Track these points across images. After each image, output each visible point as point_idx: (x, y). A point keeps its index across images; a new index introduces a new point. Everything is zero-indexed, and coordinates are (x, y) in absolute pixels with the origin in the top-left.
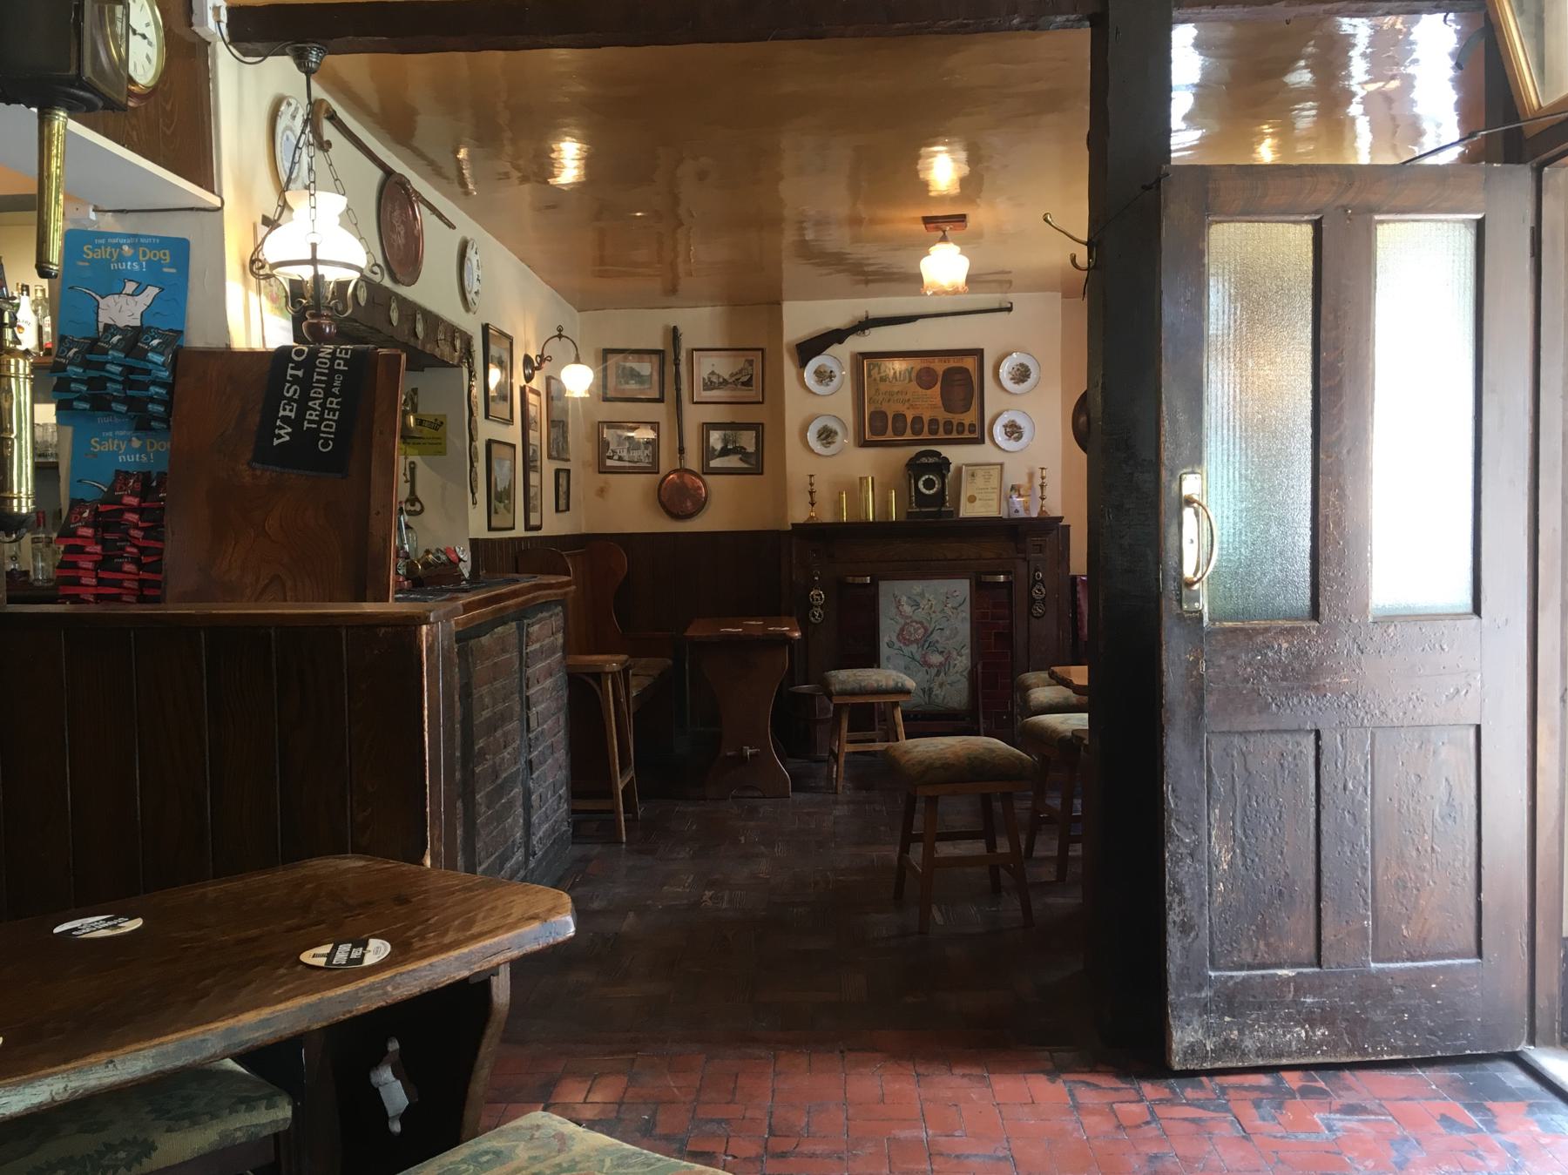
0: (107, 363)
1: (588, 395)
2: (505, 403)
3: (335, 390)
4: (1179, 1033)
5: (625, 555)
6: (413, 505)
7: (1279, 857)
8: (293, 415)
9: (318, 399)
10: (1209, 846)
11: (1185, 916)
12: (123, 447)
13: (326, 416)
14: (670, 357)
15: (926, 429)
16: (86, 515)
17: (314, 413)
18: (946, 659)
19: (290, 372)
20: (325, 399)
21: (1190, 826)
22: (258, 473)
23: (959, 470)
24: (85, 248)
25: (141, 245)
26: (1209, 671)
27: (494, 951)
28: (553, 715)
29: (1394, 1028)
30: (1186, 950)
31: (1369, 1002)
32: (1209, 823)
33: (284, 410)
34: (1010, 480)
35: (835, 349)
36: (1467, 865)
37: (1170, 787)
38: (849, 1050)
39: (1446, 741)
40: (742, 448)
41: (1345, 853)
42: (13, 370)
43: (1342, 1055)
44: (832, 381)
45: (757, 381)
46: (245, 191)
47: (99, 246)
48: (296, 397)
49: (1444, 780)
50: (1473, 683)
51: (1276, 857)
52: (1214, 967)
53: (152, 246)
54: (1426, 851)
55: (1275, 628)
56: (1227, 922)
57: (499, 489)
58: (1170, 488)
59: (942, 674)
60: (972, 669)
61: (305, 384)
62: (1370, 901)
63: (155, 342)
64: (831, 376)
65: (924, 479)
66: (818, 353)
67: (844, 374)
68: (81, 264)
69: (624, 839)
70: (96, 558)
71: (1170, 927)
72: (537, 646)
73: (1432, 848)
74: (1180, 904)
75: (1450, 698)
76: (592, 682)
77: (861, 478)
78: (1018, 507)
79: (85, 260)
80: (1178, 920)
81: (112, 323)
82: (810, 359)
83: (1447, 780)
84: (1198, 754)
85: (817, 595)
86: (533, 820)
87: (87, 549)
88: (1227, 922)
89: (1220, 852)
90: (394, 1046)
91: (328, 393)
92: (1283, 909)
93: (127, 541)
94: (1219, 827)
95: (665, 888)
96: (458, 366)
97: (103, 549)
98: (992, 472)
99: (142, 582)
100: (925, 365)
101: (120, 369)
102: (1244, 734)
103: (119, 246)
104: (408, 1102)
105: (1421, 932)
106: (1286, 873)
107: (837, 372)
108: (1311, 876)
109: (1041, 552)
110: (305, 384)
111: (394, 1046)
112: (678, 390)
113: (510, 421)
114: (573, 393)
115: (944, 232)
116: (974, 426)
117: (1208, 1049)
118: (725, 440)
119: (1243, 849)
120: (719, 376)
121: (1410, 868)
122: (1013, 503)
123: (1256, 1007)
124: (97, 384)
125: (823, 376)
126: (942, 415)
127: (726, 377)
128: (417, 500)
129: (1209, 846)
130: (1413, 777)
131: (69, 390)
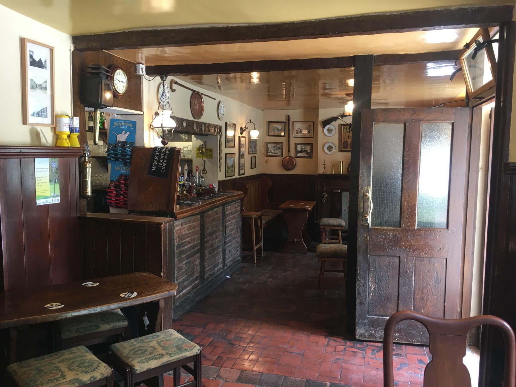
0: (118, 150)
1: (257, 139)
2: (232, 142)
3: (166, 158)
5: (271, 180)
6: (204, 171)
7: (388, 288)
8: (156, 163)
9: (162, 160)
12: (121, 169)
13: (163, 164)
14: (287, 123)
16: (113, 184)
19: (156, 153)
21: (363, 278)
24: (114, 123)
25: (126, 122)
27: (157, 297)
28: (235, 229)
29: (418, 336)
31: (411, 328)
32: (369, 278)
33: (155, 162)
35: (334, 123)
36: (442, 295)
37: (358, 268)
38: (281, 325)
39: (437, 262)
41: (406, 289)
42: (87, 166)
43: (403, 341)
44: (332, 132)
46: (150, 108)
47: (117, 123)
49: (436, 273)
50: (445, 247)
51: (387, 288)
52: (368, 315)
53: (128, 123)
54: (430, 290)
55: (389, 229)
56: (373, 304)
57: (229, 166)
61: (159, 156)
62: (413, 302)
63: (128, 145)
64: (332, 131)
66: (329, 124)
67: (336, 131)
68: (113, 126)
69: (256, 262)
70: (115, 194)
71: (357, 303)
72: (230, 212)
73: (432, 290)
75: (438, 251)
76: (249, 220)
79: (114, 126)
80: (359, 302)
82: (326, 126)
83: (437, 272)
84: (366, 260)
85: (325, 194)
86: (226, 257)
87: (113, 192)
88: (373, 304)
89: (371, 286)
90: (146, 313)
91: (164, 159)
92: (388, 302)
93: (121, 191)
95: (260, 277)
96: (217, 135)
97: (116, 192)
99: (124, 200)
101: (121, 152)
102: (379, 256)
103: (122, 123)
104: (149, 323)
105: (427, 312)
106: (389, 292)
108: (396, 294)
110: (159, 156)
111: (146, 313)
112: (289, 133)
113: (234, 147)
114: (253, 138)
117: (366, 335)
119: (378, 285)
121: (425, 295)
123: (379, 326)
124: (116, 155)
125: (329, 131)
128: (205, 170)
130: (427, 271)
131: (110, 156)
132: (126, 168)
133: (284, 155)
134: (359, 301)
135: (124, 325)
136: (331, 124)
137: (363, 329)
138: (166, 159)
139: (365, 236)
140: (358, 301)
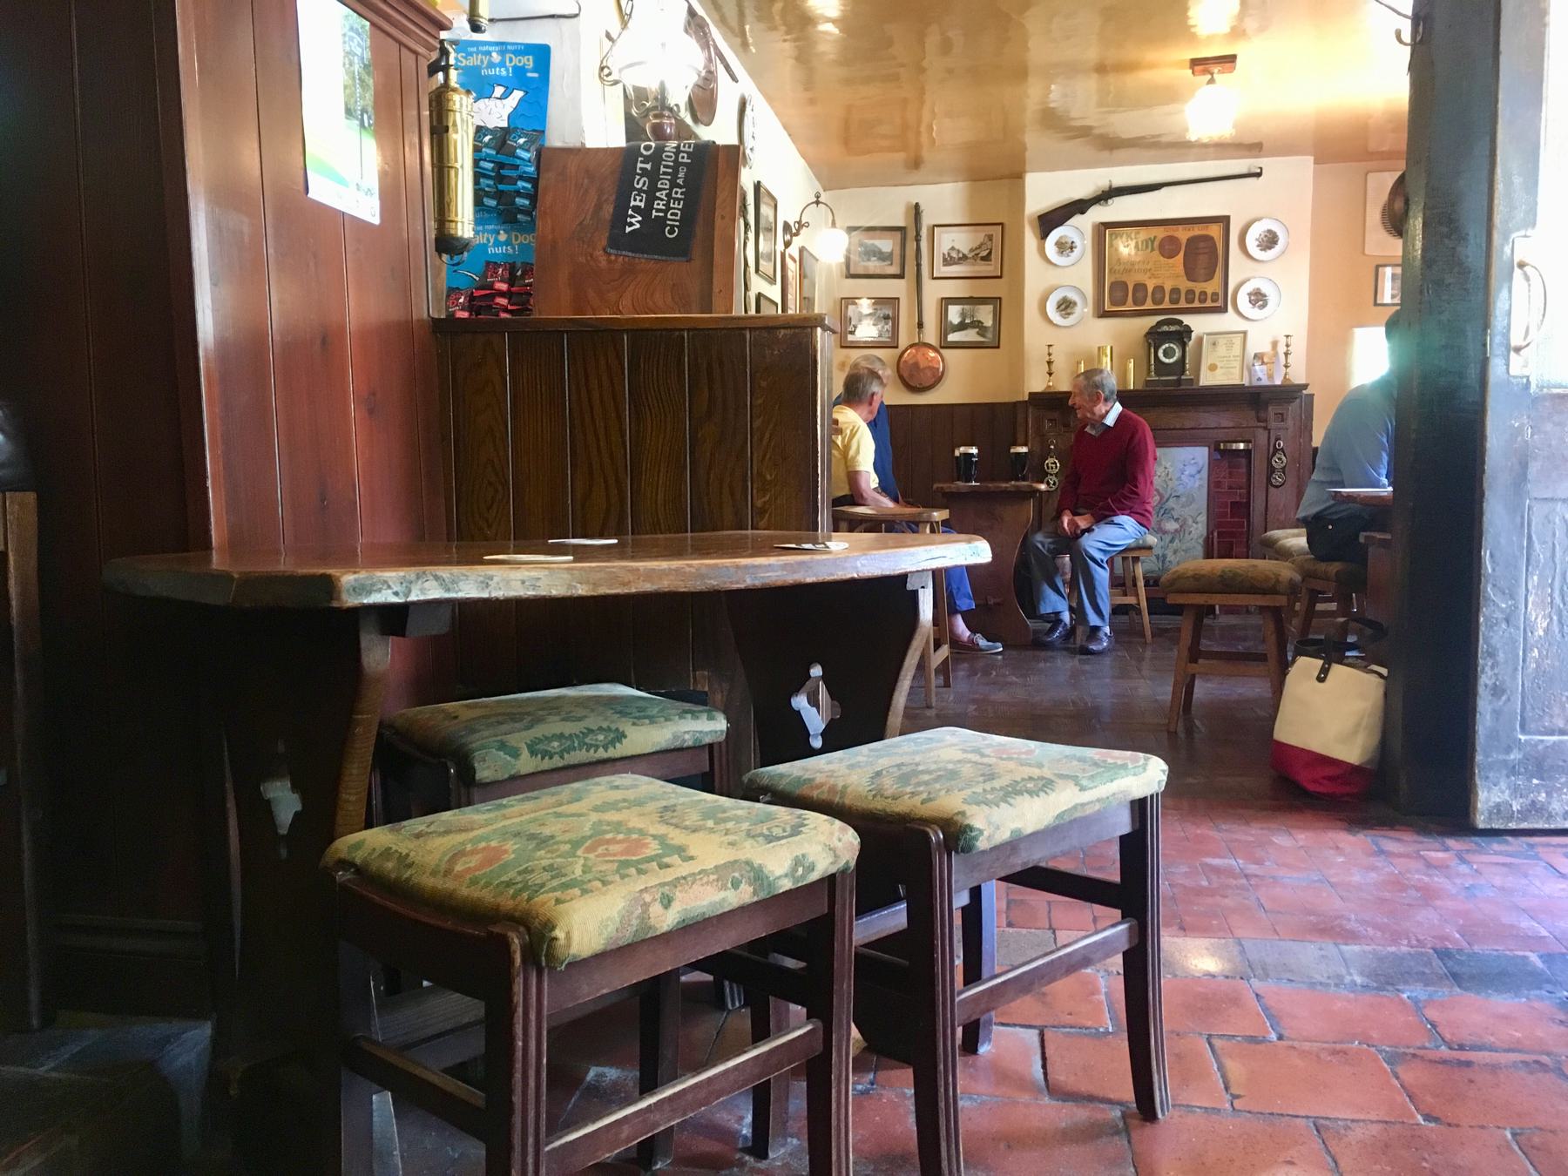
3: (680, 181)
4: (1486, 793)
8: (642, 205)
9: (665, 189)
10: (1526, 612)
11: (1497, 679)
14: (911, 234)
15: (1167, 299)
16: (461, 300)
17: (661, 203)
18: (1181, 527)
20: (671, 189)
22: (613, 258)
23: (1200, 340)
26: (1536, 437)
30: (1497, 713)
32: (1527, 590)
33: (635, 200)
34: (1252, 349)
35: (1077, 220)
40: (980, 322)
44: (1072, 251)
45: (996, 256)
47: (471, 54)
48: (645, 188)
52: (1524, 730)
58: (1502, 252)
59: (1177, 541)
60: (1208, 537)
61: (653, 176)
63: (521, 141)
65: (1164, 347)
66: (1060, 223)
71: (1481, 690)
74: (1492, 668)
77: (1099, 348)
78: (1260, 375)
80: (1490, 683)
81: (483, 124)
84: (1518, 520)
89: (1536, 619)
91: (674, 184)
94: (1536, 594)
98: (1234, 341)
100: (1169, 234)
101: (492, 165)
103: (489, 53)
107: (1078, 243)
109: (1282, 421)
112: (919, 265)
115: (1212, 74)
116: (1217, 294)
117: (1515, 809)
118: (963, 315)
120: (959, 251)
122: (1255, 371)
125: (1065, 247)
126: (1184, 284)
127: (966, 252)
129: (1526, 612)
132: (509, 239)
133: (903, 341)
134: (1490, 679)
135: (716, 732)
136: (1068, 222)
137: (1504, 788)
138: (681, 187)
139: (1516, 425)
140: (1488, 682)
